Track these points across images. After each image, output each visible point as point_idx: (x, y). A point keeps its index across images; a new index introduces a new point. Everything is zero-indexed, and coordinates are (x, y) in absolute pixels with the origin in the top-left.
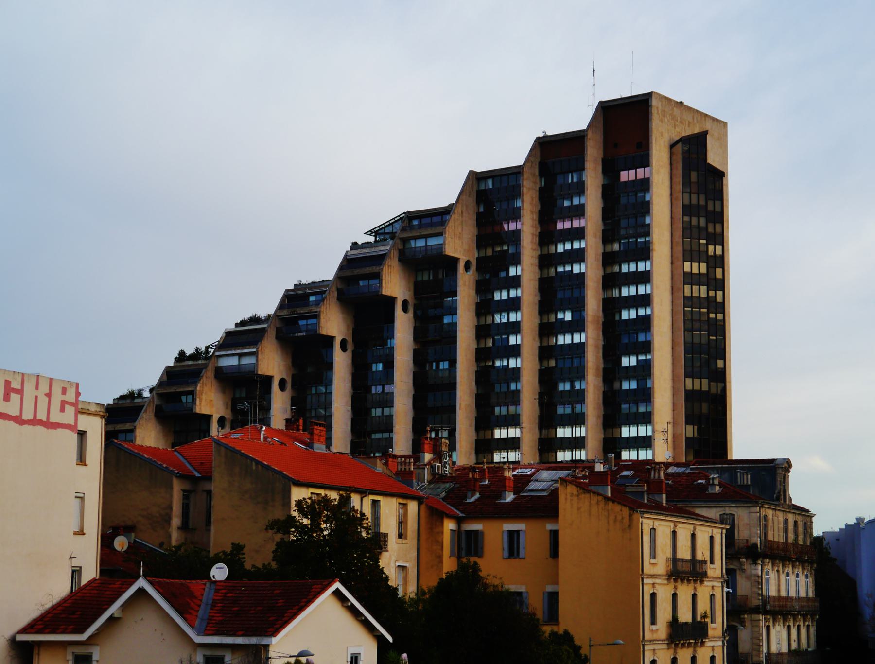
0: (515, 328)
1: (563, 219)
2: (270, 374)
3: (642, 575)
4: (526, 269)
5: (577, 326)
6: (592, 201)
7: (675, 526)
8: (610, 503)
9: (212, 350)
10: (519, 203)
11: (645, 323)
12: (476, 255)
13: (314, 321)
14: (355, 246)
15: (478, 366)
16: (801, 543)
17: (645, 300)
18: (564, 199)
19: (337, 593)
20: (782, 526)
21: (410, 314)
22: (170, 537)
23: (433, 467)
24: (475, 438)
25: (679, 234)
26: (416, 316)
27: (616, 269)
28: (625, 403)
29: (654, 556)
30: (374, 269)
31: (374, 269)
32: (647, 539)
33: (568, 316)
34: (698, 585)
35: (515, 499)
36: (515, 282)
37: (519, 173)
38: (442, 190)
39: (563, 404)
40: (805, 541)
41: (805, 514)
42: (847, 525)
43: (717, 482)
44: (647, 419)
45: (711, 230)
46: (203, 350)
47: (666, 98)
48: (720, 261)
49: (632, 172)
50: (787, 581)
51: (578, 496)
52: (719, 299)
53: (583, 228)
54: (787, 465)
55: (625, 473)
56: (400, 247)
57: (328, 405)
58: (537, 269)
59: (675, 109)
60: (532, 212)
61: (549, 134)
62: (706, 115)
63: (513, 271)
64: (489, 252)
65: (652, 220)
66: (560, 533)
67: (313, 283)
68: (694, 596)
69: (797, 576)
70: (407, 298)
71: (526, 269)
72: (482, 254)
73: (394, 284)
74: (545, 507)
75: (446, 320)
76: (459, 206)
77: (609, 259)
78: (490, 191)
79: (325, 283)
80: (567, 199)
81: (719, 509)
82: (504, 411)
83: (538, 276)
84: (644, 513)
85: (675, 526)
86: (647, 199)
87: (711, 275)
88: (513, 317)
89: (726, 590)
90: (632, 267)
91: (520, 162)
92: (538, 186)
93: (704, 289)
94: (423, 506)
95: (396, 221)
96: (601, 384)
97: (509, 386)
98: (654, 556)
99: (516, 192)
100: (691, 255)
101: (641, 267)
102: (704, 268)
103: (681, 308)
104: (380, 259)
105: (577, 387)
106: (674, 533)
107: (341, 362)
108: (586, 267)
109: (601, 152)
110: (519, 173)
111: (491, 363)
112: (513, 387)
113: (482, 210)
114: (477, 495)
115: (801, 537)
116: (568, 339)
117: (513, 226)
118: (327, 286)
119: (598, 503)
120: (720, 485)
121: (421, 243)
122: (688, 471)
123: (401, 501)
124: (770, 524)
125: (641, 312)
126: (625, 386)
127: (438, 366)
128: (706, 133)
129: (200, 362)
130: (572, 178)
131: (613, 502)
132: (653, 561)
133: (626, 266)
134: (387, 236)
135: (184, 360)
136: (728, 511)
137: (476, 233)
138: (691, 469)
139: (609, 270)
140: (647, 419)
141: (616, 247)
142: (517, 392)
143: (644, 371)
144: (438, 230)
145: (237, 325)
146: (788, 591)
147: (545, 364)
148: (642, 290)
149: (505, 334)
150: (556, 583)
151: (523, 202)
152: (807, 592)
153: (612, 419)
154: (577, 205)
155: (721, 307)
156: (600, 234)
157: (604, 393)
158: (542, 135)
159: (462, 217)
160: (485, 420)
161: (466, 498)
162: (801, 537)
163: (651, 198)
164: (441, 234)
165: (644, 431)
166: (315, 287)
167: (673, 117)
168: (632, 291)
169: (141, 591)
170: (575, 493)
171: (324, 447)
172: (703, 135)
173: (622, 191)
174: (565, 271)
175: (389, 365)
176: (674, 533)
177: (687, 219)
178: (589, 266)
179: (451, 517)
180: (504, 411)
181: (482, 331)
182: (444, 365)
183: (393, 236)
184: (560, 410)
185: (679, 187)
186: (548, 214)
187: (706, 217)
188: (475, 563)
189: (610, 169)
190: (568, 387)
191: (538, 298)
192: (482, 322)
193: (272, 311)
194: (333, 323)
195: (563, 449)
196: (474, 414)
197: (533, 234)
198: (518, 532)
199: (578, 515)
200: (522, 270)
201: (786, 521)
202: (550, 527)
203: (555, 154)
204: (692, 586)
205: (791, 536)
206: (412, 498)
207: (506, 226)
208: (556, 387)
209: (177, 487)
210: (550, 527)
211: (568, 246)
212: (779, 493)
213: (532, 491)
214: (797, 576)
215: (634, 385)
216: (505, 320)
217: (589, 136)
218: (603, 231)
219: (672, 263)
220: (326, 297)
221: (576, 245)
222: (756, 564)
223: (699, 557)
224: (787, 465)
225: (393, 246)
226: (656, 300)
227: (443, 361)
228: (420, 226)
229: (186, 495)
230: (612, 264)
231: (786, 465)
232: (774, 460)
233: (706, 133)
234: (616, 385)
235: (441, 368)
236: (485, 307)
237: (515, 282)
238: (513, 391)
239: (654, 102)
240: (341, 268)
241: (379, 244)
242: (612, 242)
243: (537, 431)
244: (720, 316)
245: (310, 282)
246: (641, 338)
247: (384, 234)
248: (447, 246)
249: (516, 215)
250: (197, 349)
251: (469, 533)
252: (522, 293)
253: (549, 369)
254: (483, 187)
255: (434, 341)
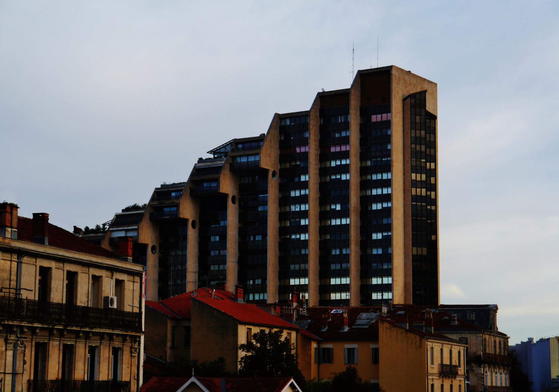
0: (304, 215)
1: (335, 145)
2: (146, 242)
3: (427, 374)
4: (310, 177)
5: (344, 213)
6: (354, 134)
7: (442, 346)
8: (409, 333)
9: (108, 227)
10: (307, 135)
11: (388, 212)
12: (279, 168)
13: (174, 209)
14: (201, 160)
15: (280, 238)
16: (502, 354)
17: (388, 198)
18: (336, 132)
19: (292, 386)
20: (493, 344)
21: (237, 205)
22: (166, 352)
23: (298, 311)
24: (278, 284)
25: (408, 155)
26: (240, 206)
27: (369, 177)
28: (375, 262)
29: (432, 363)
30: (215, 176)
31: (215, 176)
32: (429, 353)
33: (338, 207)
34: (453, 380)
35: (349, 330)
36: (305, 185)
37: (308, 115)
38: (259, 126)
39: (335, 263)
40: (504, 352)
41: (505, 337)
42: (522, 342)
43: (456, 318)
44: (389, 273)
45: (428, 152)
46: (101, 226)
47: (401, 69)
48: (433, 173)
49: (379, 116)
50: (496, 377)
51: (390, 329)
52: (433, 197)
53: (349, 151)
54: (494, 309)
55: (400, 312)
56: (231, 162)
57: (184, 262)
58: (318, 177)
59: (406, 76)
60: (315, 141)
61: (326, 90)
62: (425, 79)
63: (303, 178)
64: (288, 166)
65: (392, 146)
66: (380, 350)
67: (174, 184)
68: (451, 386)
69: (501, 374)
70: (235, 194)
71: (310, 177)
72: (283, 167)
73: (227, 186)
74: (370, 334)
75: (260, 209)
76: (269, 136)
77: (364, 171)
78: (288, 127)
79: (183, 185)
80: (338, 133)
81: (458, 335)
82: (297, 267)
83: (319, 181)
84: (428, 339)
85: (442, 346)
86: (389, 133)
87: (428, 182)
88: (303, 207)
89: (467, 382)
90: (379, 177)
91: (308, 109)
92: (319, 124)
93: (424, 190)
94: (299, 334)
95: (227, 145)
96: (359, 251)
97: (300, 252)
98: (432, 363)
99: (305, 127)
100: (415, 170)
101: (385, 176)
102: (424, 177)
103: (409, 203)
104: (218, 170)
105: (344, 252)
106: (442, 350)
107: (192, 234)
108: (350, 176)
109: (359, 103)
110: (308, 115)
111: (289, 237)
112: (303, 252)
113: (283, 138)
114: (327, 328)
115: (502, 351)
116: (338, 222)
117: (303, 149)
118: (184, 186)
119: (402, 333)
120: (458, 320)
121: (244, 160)
122: (437, 312)
123: (288, 331)
124: (487, 344)
125: (385, 205)
126: (375, 252)
127: (254, 238)
128: (425, 92)
129: (99, 234)
130: (341, 119)
131: (411, 332)
132: (432, 366)
133: (375, 176)
134: (221, 155)
135: (89, 233)
136: (464, 336)
137: (279, 153)
138: (439, 310)
139: (364, 178)
140: (389, 273)
141: (369, 163)
142: (306, 256)
143: (387, 242)
144: (256, 151)
145: (123, 211)
146: (496, 383)
147: (323, 237)
148: (385, 191)
149: (298, 218)
150: (378, 378)
151: (310, 134)
152: (506, 383)
153: (366, 273)
154: (344, 137)
155: (434, 202)
156: (358, 155)
157: (361, 256)
158: (321, 91)
159: (271, 143)
160: (284, 274)
161: (320, 329)
162: (502, 351)
163: (392, 132)
164: (258, 154)
165: (387, 280)
166: (175, 187)
167: (405, 81)
168: (379, 191)
169: (193, 384)
170: (389, 327)
171: (242, 300)
172: (423, 93)
173: (373, 127)
174: (336, 179)
175: (224, 237)
176: (442, 350)
177: (413, 146)
178: (352, 175)
179: (315, 340)
180: (297, 267)
181: (283, 216)
182: (259, 238)
183: (226, 154)
184: (333, 267)
185: (408, 126)
186: (325, 142)
187: (426, 145)
188: (354, 368)
189: (365, 114)
190: (338, 252)
191: (319, 195)
192: (283, 210)
193: (147, 202)
194: (187, 211)
195: (335, 292)
196: (278, 269)
197: (316, 155)
198: (353, 349)
199: (390, 341)
200: (309, 177)
201: (495, 341)
202: (372, 346)
203: (330, 103)
204: (450, 380)
205: (498, 350)
206: (293, 329)
207: (298, 150)
208: (330, 252)
209: (169, 325)
210: (372, 346)
211: (338, 163)
212: (491, 325)
213: (358, 325)
214: (501, 374)
215: (380, 251)
216: (298, 209)
217: (352, 93)
218: (360, 153)
219: (404, 174)
220: (183, 194)
221: (344, 162)
222: (480, 367)
223: (454, 363)
224: (494, 309)
225: (226, 161)
226: (394, 198)
227: (258, 235)
228: (243, 149)
229: (174, 328)
230: (366, 174)
231: (495, 308)
232: (487, 306)
233: (425, 92)
234: (369, 251)
235: (257, 239)
236: (285, 201)
237: (305, 185)
238: (303, 255)
239: (394, 72)
240: (192, 175)
241: (217, 160)
242: (366, 160)
243: (318, 280)
244: (433, 208)
245: (171, 183)
246: (385, 221)
247: (220, 153)
248: (262, 162)
249: (305, 142)
250: (98, 227)
251: (324, 349)
252: (309, 192)
253: (326, 240)
254: (283, 124)
255: (252, 222)
